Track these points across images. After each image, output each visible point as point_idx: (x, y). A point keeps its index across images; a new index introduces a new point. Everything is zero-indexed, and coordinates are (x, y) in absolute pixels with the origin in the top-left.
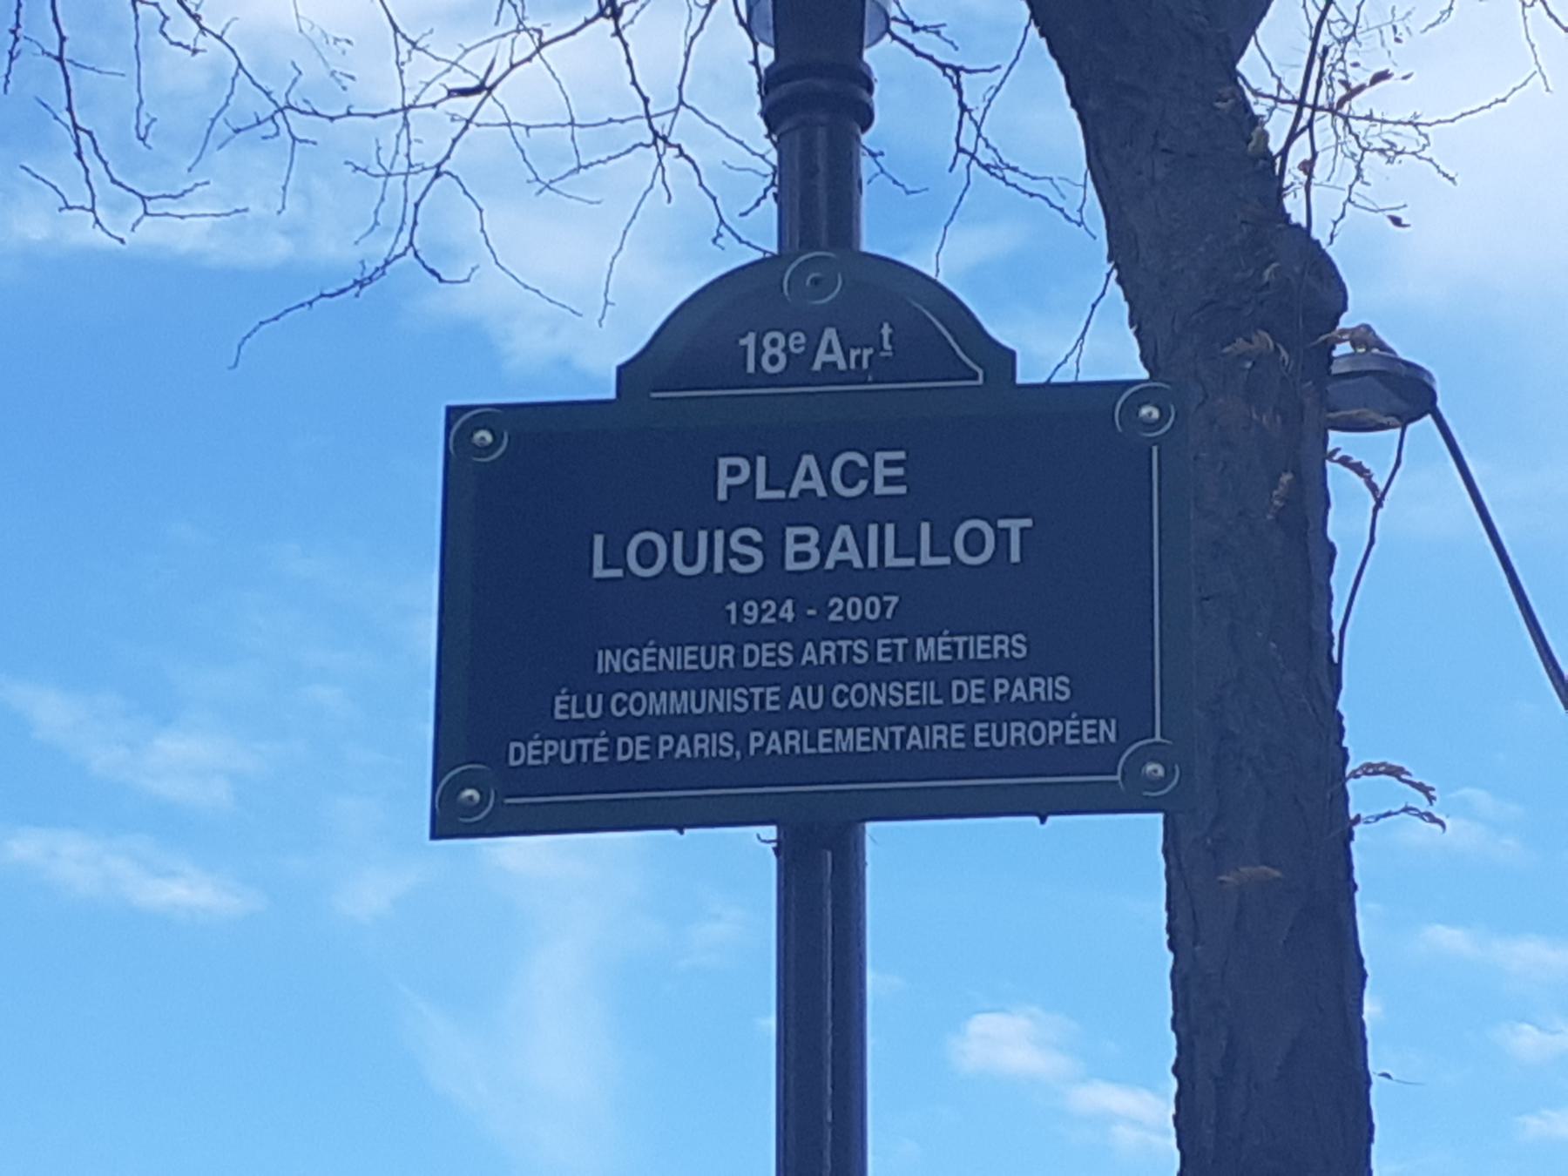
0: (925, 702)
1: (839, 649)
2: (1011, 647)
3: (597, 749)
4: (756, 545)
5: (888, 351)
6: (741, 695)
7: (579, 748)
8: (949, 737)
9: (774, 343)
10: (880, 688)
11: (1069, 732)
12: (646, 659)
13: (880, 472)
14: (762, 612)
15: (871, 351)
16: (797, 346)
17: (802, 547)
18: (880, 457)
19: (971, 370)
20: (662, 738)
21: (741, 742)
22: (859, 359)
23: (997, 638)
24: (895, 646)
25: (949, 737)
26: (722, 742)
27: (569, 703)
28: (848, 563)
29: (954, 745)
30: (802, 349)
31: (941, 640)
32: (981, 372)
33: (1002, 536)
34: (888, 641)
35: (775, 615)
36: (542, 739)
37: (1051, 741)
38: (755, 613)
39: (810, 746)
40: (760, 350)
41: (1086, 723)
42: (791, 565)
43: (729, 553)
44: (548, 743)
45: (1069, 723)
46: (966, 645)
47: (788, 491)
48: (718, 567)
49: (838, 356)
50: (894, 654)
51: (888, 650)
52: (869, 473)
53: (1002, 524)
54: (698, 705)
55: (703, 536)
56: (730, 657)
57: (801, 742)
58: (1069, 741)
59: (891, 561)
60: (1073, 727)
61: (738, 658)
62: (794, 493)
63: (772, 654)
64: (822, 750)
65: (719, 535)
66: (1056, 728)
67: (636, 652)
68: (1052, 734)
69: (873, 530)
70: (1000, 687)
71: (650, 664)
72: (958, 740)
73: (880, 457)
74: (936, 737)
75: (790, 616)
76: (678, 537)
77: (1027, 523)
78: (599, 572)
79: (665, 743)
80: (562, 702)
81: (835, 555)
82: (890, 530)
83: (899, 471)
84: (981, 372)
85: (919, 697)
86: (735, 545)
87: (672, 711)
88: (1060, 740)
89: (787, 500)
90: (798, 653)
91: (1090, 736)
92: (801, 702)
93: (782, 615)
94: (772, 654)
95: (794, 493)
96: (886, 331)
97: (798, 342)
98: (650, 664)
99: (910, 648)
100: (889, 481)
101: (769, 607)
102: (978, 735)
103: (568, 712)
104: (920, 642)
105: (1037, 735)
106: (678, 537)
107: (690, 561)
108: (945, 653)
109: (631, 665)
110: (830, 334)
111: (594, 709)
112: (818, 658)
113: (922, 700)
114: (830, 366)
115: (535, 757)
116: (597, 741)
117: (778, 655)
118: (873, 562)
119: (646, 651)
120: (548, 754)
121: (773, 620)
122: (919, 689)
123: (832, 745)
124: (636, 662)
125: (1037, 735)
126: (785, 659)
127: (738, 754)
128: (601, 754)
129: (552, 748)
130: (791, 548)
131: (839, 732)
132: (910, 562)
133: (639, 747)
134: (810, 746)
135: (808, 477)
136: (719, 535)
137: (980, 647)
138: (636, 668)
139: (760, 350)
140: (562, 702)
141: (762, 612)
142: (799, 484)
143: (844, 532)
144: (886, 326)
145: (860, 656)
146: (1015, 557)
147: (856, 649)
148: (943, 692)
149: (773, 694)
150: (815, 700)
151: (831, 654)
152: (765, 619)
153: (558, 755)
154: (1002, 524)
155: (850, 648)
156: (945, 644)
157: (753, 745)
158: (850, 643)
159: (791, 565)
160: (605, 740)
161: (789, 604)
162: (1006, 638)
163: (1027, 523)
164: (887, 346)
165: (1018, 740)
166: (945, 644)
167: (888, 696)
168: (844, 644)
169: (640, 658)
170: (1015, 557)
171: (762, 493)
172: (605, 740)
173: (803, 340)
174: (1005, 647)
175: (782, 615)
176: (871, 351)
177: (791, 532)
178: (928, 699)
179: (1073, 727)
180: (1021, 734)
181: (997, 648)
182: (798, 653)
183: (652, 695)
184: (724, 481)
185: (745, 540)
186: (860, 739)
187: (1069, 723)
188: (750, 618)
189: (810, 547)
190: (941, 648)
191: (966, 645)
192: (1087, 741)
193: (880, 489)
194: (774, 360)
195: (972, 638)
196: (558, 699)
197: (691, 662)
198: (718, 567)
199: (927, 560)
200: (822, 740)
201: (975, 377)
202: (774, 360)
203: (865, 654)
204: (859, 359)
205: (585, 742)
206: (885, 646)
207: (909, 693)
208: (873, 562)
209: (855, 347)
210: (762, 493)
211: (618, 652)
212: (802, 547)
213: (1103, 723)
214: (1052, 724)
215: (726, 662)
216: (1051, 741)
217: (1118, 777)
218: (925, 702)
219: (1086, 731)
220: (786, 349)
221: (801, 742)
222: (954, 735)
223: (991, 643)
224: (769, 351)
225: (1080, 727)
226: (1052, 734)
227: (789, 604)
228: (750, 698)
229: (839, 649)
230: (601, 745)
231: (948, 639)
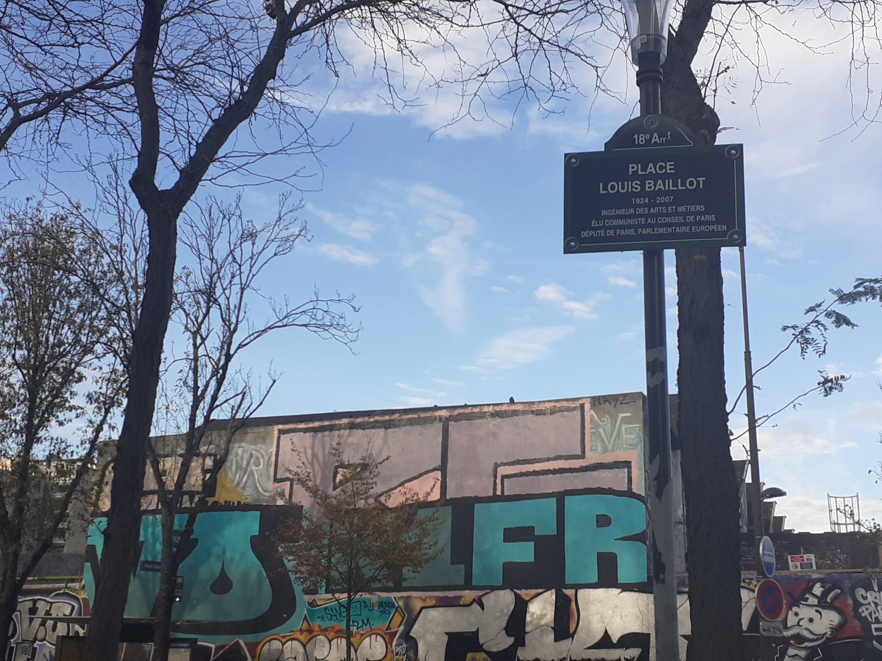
13: (668, 167)
21: (636, 231)
33: (698, 182)
40: (638, 139)
42: (647, 189)
43: (632, 187)
49: (657, 140)
52: (666, 167)
55: (626, 183)
59: (671, 188)
65: (630, 183)
69: (667, 181)
77: (704, 179)
78: (601, 192)
79: (618, 232)
83: (673, 167)
90: (649, 210)
96: (669, 133)
99: (676, 209)
100: (670, 169)
106: (620, 183)
107: (623, 189)
110: (655, 135)
114: (656, 142)
118: (667, 189)
129: (591, 233)
130: (647, 185)
132: (676, 188)
136: (630, 183)
139: (638, 139)
143: (660, 181)
146: (701, 187)
148: (684, 219)
159: (647, 189)
170: (701, 187)
171: (640, 172)
177: (647, 182)
182: (649, 210)
184: (631, 170)
185: (636, 184)
193: (668, 171)
198: (630, 190)
199: (680, 188)
202: (642, 141)
224: (641, 139)
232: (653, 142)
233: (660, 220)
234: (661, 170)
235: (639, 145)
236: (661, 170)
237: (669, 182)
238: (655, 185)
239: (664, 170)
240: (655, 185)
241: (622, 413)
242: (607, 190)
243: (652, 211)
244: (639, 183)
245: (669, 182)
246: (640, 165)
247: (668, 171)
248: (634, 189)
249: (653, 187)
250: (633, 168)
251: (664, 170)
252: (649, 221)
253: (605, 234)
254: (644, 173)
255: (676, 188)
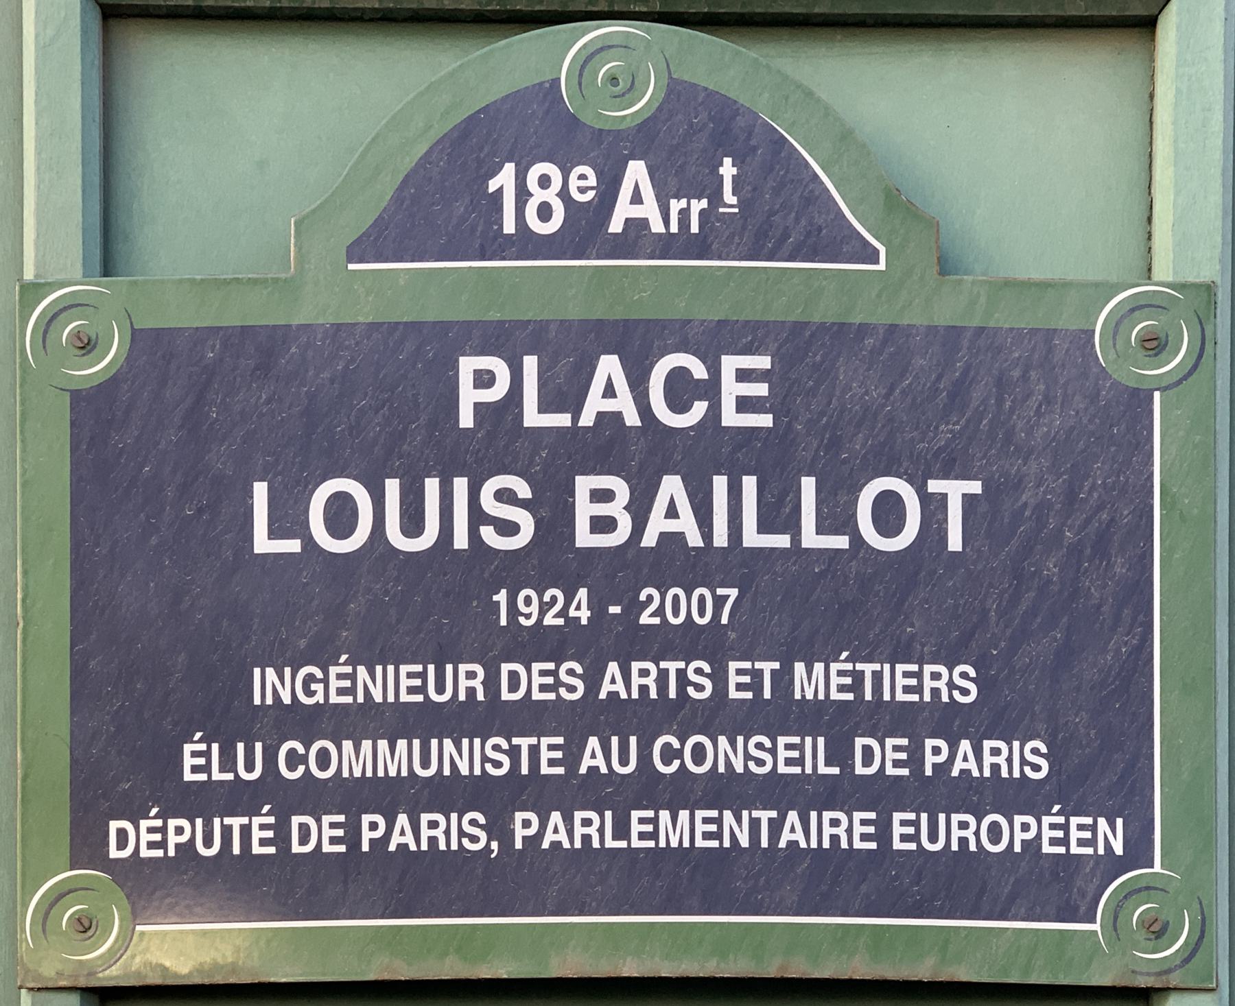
0: (809, 770)
1: (663, 675)
2: (951, 685)
3: (257, 834)
4: (523, 504)
5: (732, 206)
6: (496, 748)
7: (227, 831)
8: (849, 831)
9: (544, 182)
10: (733, 744)
11: (1047, 834)
12: (334, 684)
13: (731, 389)
14: (544, 608)
15: (704, 203)
16: (582, 190)
17: (602, 509)
18: (730, 364)
19: (866, 243)
20: (366, 819)
21: (499, 828)
22: (684, 214)
23: (928, 669)
24: (757, 675)
25: (849, 831)
26: (467, 828)
27: (207, 754)
28: (680, 537)
29: (858, 845)
30: (590, 195)
31: (834, 667)
32: (882, 250)
33: (934, 507)
34: (747, 665)
35: (563, 613)
36: (163, 815)
37: (1017, 848)
38: (534, 609)
39: (615, 837)
40: (523, 194)
41: (1075, 821)
42: (584, 538)
43: (477, 516)
44: (172, 823)
45: (1046, 820)
46: (877, 676)
47: (576, 419)
48: (461, 541)
49: (649, 210)
50: (756, 686)
51: (746, 679)
52: (711, 390)
53: (934, 486)
54: (425, 764)
55: (432, 486)
56: (477, 684)
57: (601, 831)
58: (1047, 849)
59: (752, 538)
60: (1053, 827)
61: (491, 683)
62: (587, 419)
63: (550, 680)
64: (636, 843)
65: (461, 485)
66: (1025, 827)
67: (319, 674)
68: (1019, 836)
69: (720, 484)
70: (934, 750)
71: (341, 692)
72: (864, 838)
73: (730, 364)
74: (828, 831)
75: (584, 615)
76: (392, 487)
77: (975, 487)
78: (262, 543)
79: (371, 827)
80: (195, 754)
81: (657, 525)
82: (750, 484)
83: (761, 389)
84: (882, 250)
85: (800, 762)
86: (489, 504)
87: (381, 774)
88: (1032, 846)
89: (575, 430)
90: (593, 679)
91: (1081, 843)
92: (600, 762)
93: (572, 613)
94: (550, 680)
95: (587, 419)
96: (728, 170)
97: (583, 183)
98: (341, 692)
99: (783, 679)
100: (744, 405)
101: (554, 599)
102: (897, 830)
103: (206, 768)
104: (800, 668)
105: (995, 830)
106: (392, 487)
107: (413, 525)
108: (842, 688)
109: (310, 693)
110: (636, 171)
111: (250, 767)
112: (418, 841)
113: (803, 766)
114: (637, 226)
115: (152, 845)
116: (256, 821)
117: (558, 683)
118: (721, 538)
119: (333, 670)
120: (173, 840)
121: (560, 621)
122: (800, 747)
123: (654, 835)
124: (318, 687)
125: (995, 830)
126: (572, 689)
127: (494, 845)
128: (263, 842)
129: (181, 829)
130: (584, 510)
131: (665, 815)
132: (782, 541)
133: (327, 833)
134: (615, 837)
135: (609, 392)
136: (461, 485)
137: (901, 682)
138: (320, 698)
139: (523, 194)
140: (195, 754)
141: (544, 608)
142: (594, 405)
143: (672, 486)
144: (728, 161)
145: (699, 688)
146: (955, 542)
147: (692, 677)
148: (839, 753)
149: (551, 747)
150: (624, 761)
151: (650, 681)
152: (549, 620)
153: (192, 839)
154: (934, 486)
155: (681, 674)
156: (841, 673)
157: (520, 833)
158: (682, 665)
159: (584, 538)
160: (271, 820)
161: (582, 593)
162: (942, 669)
163: (975, 487)
164: (729, 197)
165: (963, 841)
166: (841, 673)
167: (748, 758)
168: (672, 666)
169: (325, 681)
170: (955, 542)
171: (533, 417)
172: (271, 820)
173: (592, 181)
174: (941, 684)
175: (572, 613)
176: (704, 203)
177: (584, 484)
178: (815, 767)
179: (1053, 827)
180: (969, 833)
181: (928, 684)
182: (593, 679)
183: (348, 745)
184: (469, 397)
185: (505, 496)
186: (700, 828)
187: (1046, 820)
188: (528, 616)
189: (617, 509)
190: (835, 680)
191: (877, 676)
192: (1075, 850)
193: (731, 418)
194: (545, 212)
195: (887, 667)
196: (188, 748)
197: (411, 690)
198: (461, 541)
199: (811, 539)
200: (636, 828)
201: (873, 257)
202: (545, 212)
203: (708, 684)
204: (684, 214)
205: (236, 822)
206: (739, 672)
207: (783, 754)
208: (721, 538)
209: (678, 198)
210: (533, 417)
211: (288, 671)
212: (602, 509)
213: (1102, 823)
214: (1019, 819)
215: (471, 692)
216: (1017, 848)
217: (1096, 927)
218: (809, 770)
219: (1075, 834)
220: (564, 194)
221: (601, 831)
222: (858, 829)
223: (919, 675)
224: (539, 196)
225: (1065, 827)
226: (1019, 836)
227: (582, 593)
228: (514, 752)
229: (663, 675)
230: (263, 827)
231: (849, 666)
232: (616, 226)
233: (669, 754)
234: (678, 404)
235: (526, 243)
236: (678, 404)
237: (735, 493)
238: (640, 510)
239: (699, 409)
240: (640, 510)
241: (330, 813)
242: (659, 669)
243: (612, 682)
244: (524, 490)
245: (735, 493)
246: (530, 363)
247: (731, 418)
248: (488, 534)
249: (625, 525)
250: (484, 379)
251: (699, 409)
252: (592, 757)
253: (281, 836)
254: (562, 420)
255: (782, 541)
